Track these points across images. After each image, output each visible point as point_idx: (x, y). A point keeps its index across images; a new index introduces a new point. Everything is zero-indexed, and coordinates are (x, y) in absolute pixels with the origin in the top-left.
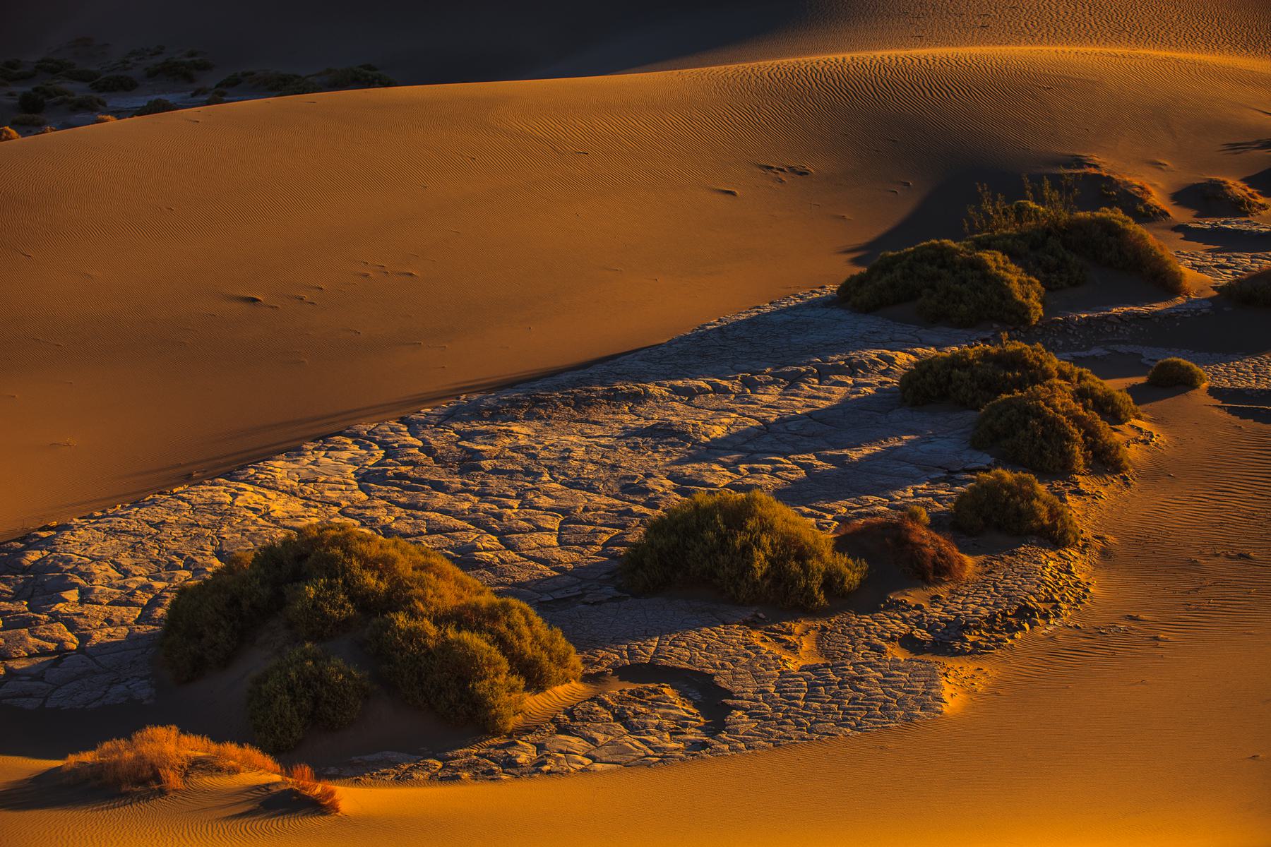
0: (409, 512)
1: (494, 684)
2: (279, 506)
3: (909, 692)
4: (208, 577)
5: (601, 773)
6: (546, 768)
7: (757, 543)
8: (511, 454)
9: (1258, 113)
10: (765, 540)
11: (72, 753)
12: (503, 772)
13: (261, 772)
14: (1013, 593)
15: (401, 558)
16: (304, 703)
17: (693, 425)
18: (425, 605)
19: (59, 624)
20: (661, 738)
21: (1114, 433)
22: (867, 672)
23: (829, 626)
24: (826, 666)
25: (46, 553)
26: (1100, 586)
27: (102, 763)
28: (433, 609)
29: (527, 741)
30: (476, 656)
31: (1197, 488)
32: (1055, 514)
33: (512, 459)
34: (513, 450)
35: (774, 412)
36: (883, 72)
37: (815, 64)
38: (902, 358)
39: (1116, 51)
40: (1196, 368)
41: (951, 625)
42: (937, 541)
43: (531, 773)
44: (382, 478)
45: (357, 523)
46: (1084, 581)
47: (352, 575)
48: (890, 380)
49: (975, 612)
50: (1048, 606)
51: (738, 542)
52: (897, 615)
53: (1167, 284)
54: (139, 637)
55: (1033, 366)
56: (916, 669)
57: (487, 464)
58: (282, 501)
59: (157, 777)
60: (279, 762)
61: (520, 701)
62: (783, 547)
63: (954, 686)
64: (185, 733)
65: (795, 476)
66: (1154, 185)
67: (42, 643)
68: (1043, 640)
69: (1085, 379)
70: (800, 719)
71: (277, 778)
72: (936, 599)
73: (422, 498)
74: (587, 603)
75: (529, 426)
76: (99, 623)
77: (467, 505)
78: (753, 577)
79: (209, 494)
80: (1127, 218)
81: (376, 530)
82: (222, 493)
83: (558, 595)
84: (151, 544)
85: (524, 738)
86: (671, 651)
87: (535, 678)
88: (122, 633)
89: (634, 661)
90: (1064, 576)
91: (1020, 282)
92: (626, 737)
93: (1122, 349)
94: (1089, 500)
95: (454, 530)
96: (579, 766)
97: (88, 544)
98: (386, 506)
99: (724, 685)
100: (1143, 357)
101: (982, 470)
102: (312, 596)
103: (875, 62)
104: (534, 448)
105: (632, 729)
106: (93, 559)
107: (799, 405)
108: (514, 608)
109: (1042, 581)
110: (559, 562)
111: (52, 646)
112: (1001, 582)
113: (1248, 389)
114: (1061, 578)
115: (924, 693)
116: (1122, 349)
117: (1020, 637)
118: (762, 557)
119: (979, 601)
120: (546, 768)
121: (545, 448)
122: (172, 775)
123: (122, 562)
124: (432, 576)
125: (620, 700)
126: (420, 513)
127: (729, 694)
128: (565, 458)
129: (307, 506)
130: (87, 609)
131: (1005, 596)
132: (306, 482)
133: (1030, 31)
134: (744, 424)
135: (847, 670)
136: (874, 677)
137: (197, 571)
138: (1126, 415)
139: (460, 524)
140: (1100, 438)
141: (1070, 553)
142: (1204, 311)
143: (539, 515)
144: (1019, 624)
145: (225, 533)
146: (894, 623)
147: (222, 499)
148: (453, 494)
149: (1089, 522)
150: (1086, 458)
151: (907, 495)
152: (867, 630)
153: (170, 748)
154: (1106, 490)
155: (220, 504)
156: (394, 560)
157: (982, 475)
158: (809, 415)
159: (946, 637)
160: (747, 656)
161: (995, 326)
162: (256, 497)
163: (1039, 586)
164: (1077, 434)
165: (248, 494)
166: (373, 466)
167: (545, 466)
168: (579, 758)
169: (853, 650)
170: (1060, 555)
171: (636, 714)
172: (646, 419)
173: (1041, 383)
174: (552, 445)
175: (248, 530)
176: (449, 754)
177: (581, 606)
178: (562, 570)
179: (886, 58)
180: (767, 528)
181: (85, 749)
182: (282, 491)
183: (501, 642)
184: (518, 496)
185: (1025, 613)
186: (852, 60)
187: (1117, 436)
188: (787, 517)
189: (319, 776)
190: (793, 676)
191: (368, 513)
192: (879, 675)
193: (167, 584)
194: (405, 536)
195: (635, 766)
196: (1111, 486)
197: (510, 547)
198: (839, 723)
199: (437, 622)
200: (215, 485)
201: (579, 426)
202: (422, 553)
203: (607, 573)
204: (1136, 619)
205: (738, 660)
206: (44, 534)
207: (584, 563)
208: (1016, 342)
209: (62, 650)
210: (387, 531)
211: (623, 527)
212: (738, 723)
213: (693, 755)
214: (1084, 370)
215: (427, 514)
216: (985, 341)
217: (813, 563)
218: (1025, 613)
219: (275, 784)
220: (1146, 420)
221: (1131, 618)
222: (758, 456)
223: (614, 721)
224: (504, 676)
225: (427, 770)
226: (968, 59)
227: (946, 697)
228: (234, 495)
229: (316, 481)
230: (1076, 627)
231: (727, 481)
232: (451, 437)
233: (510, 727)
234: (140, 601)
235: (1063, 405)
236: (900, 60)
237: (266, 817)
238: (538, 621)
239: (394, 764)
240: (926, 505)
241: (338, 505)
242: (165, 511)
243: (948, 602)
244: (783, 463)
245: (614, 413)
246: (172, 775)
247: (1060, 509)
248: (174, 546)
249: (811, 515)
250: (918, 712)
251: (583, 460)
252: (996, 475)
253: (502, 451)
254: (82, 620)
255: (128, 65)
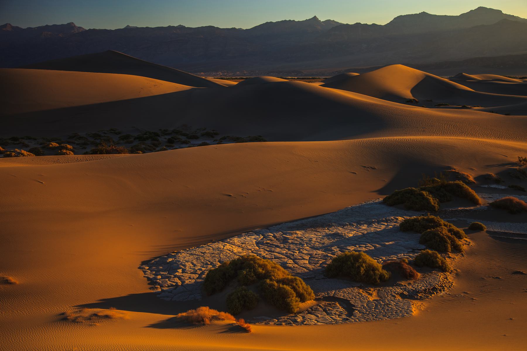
0: (270, 253)
1: (292, 299)
2: (236, 250)
3: (403, 309)
4: (217, 267)
5: (319, 325)
6: (305, 323)
7: (362, 266)
8: (296, 239)
9: (502, 156)
10: (364, 265)
11: (180, 313)
12: (294, 324)
13: (231, 320)
14: (432, 284)
15: (268, 265)
16: (242, 302)
17: (344, 234)
18: (274, 278)
19: (176, 278)
20: (336, 317)
21: (459, 242)
22: (391, 302)
23: (381, 289)
24: (380, 300)
25: (173, 259)
26: (456, 283)
27: (188, 316)
28: (276, 278)
29: (300, 315)
30: (287, 292)
31: (483, 258)
32: (443, 263)
33: (297, 240)
34: (297, 238)
35: (366, 231)
36: (396, 143)
37: (378, 140)
38: (400, 219)
39: (461, 138)
40: (483, 225)
41: (414, 291)
42: (410, 268)
43: (301, 324)
44: (263, 244)
45: (256, 255)
46: (451, 282)
47: (256, 269)
48: (397, 224)
49: (420, 288)
50: (441, 288)
51: (357, 265)
52: (399, 287)
53: (475, 202)
54: (198, 282)
55: (436, 222)
56: (405, 303)
57: (290, 241)
58: (236, 248)
59: (203, 320)
60: (235, 318)
61: (298, 305)
62: (369, 267)
63: (415, 308)
64: (211, 309)
65: (371, 248)
66: (471, 175)
67: (172, 283)
68: (439, 297)
69: (451, 226)
70: (373, 314)
71: (235, 322)
72: (409, 284)
73: (273, 249)
74: (316, 279)
75: (301, 232)
76: (187, 278)
77: (285, 252)
78: (360, 275)
79: (217, 245)
80: (464, 183)
81: (261, 257)
82: (221, 245)
83: (309, 277)
84: (202, 258)
85: (299, 315)
86: (338, 293)
87: (302, 298)
88: (193, 281)
89: (329, 296)
90: (446, 280)
91: (433, 200)
92: (326, 316)
93: (461, 219)
94: (452, 259)
95: (281, 258)
96: (314, 323)
97: (185, 257)
98: (264, 251)
99: (352, 303)
100: (467, 221)
101: (423, 250)
102: (245, 273)
103: (394, 140)
104: (302, 238)
105: (328, 314)
106: (186, 261)
107: (373, 230)
108: (297, 279)
109: (439, 281)
110: (309, 268)
111: (174, 284)
112: (428, 280)
113: (498, 232)
114: (445, 280)
115: (407, 309)
116: (461, 219)
117: (433, 296)
118: (363, 269)
119: (422, 285)
120: (305, 323)
121: (305, 238)
122: (207, 320)
123: (194, 263)
124: (276, 270)
125: (325, 306)
126: (272, 253)
127: (354, 306)
128: (310, 241)
129: (243, 250)
130: (184, 274)
131: (429, 284)
132: (243, 243)
133: (437, 132)
134: (358, 234)
135: (386, 301)
136: (393, 304)
137: (214, 266)
138: (463, 237)
139: (283, 256)
140: (456, 243)
141: (447, 274)
142: (485, 210)
143: (304, 255)
144: (433, 292)
145: (221, 256)
146: (398, 289)
147: (221, 247)
148: (281, 249)
149: (452, 265)
150: (451, 248)
151: (402, 255)
152: (391, 291)
153: (207, 313)
154: (457, 257)
155: (220, 248)
156: (267, 265)
157: (423, 251)
158: (375, 232)
159: (413, 294)
160: (358, 296)
161: (426, 211)
162: (229, 247)
163: (438, 282)
164: (449, 241)
165: (227, 246)
166: (260, 240)
167: (305, 242)
168: (314, 321)
169: (387, 296)
170: (444, 274)
171: (329, 310)
172: (332, 231)
173: (439, 227)
174: (307, 237)
175: (227, 255)
176: (279, 318)
177: (315, 280)
178: (310, 270)
179: (397, 139)
180: (364, 262)
181: (183, 312)
182: (237, 246)
183: (294, 288)
184: (298, 250)
185: (434, 289)
186: (388, 139)
187: (460, 242)
188: (369, 259)
189: (246, 322)
190: (371, 302)
191: (259, 252)
192: (395, 303)
193: (205, 269)
194: (269, 259)
195: (329, 324)
196: (458, 256)
197: (296, 263)
198: (384, 316)
199: (277, 282)
200: (219, 243)
201: (314, 232)
202: (274, 264)
203: (321, 272)
204: (467, 293)
205: (356, 297)
206: (173, 254)
207: (315, 268)
208: (432, 216)
209: (177, 285)
210: (264, 258)
211: (326, 259)
212: (356, 314)
213: (344, 322)
214: (451, 224)
215: (274, 253)
216: (423, 215)
217: (377, 272)
218: (434, 289)
219: (234, 324)
220: (468, 238)
221: (465, 293)
222: (361, 243)
223: (323, 311)
224: (295, 297)
225: (274, 322)
226: (419, 139)
227: (413, 311)
228: (224, 246)
229: (245, 243)
230: (449, 294)
231: (353, 249)
232: (281, 234)
233: (296, 311)
234: (198, 273)
235: (445, 233)
236: (401, 139)
237: (231, 333)
238: (304, 283)
239: (265, 320)
240: (407, 258)
241: (251, 250)
242: (206, 249)
243: (413, 285)
244: (368, 245)
245: (323, 229)
246: (207, 320)
247: (444, 261)
248: (208, 259)
249: (376, 259)
250: (405, 314)
251: (315, 241)
252: (427, 251)
253: (294, 238)
254: (183, 277)
255: (197, 132)
